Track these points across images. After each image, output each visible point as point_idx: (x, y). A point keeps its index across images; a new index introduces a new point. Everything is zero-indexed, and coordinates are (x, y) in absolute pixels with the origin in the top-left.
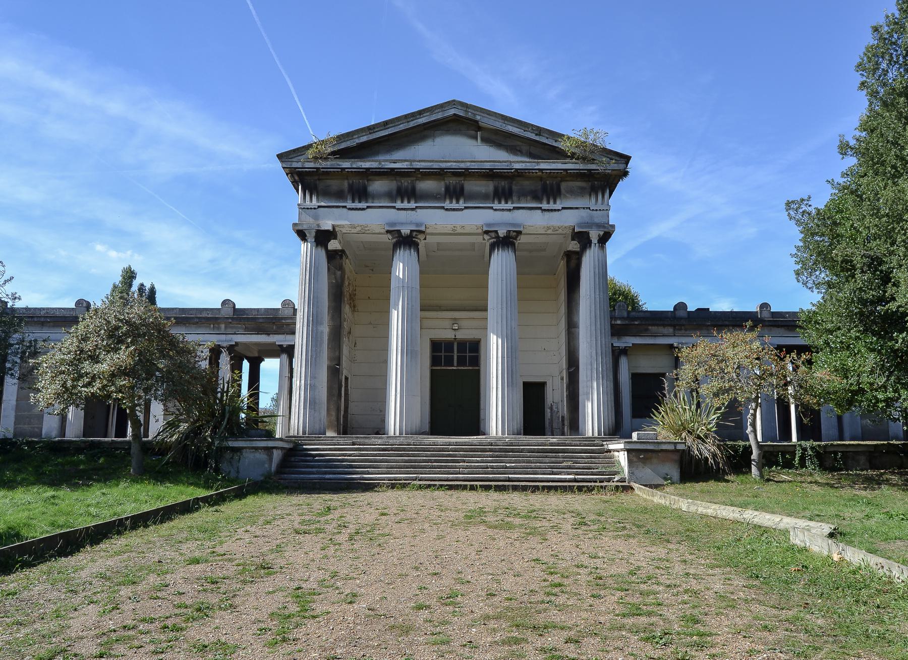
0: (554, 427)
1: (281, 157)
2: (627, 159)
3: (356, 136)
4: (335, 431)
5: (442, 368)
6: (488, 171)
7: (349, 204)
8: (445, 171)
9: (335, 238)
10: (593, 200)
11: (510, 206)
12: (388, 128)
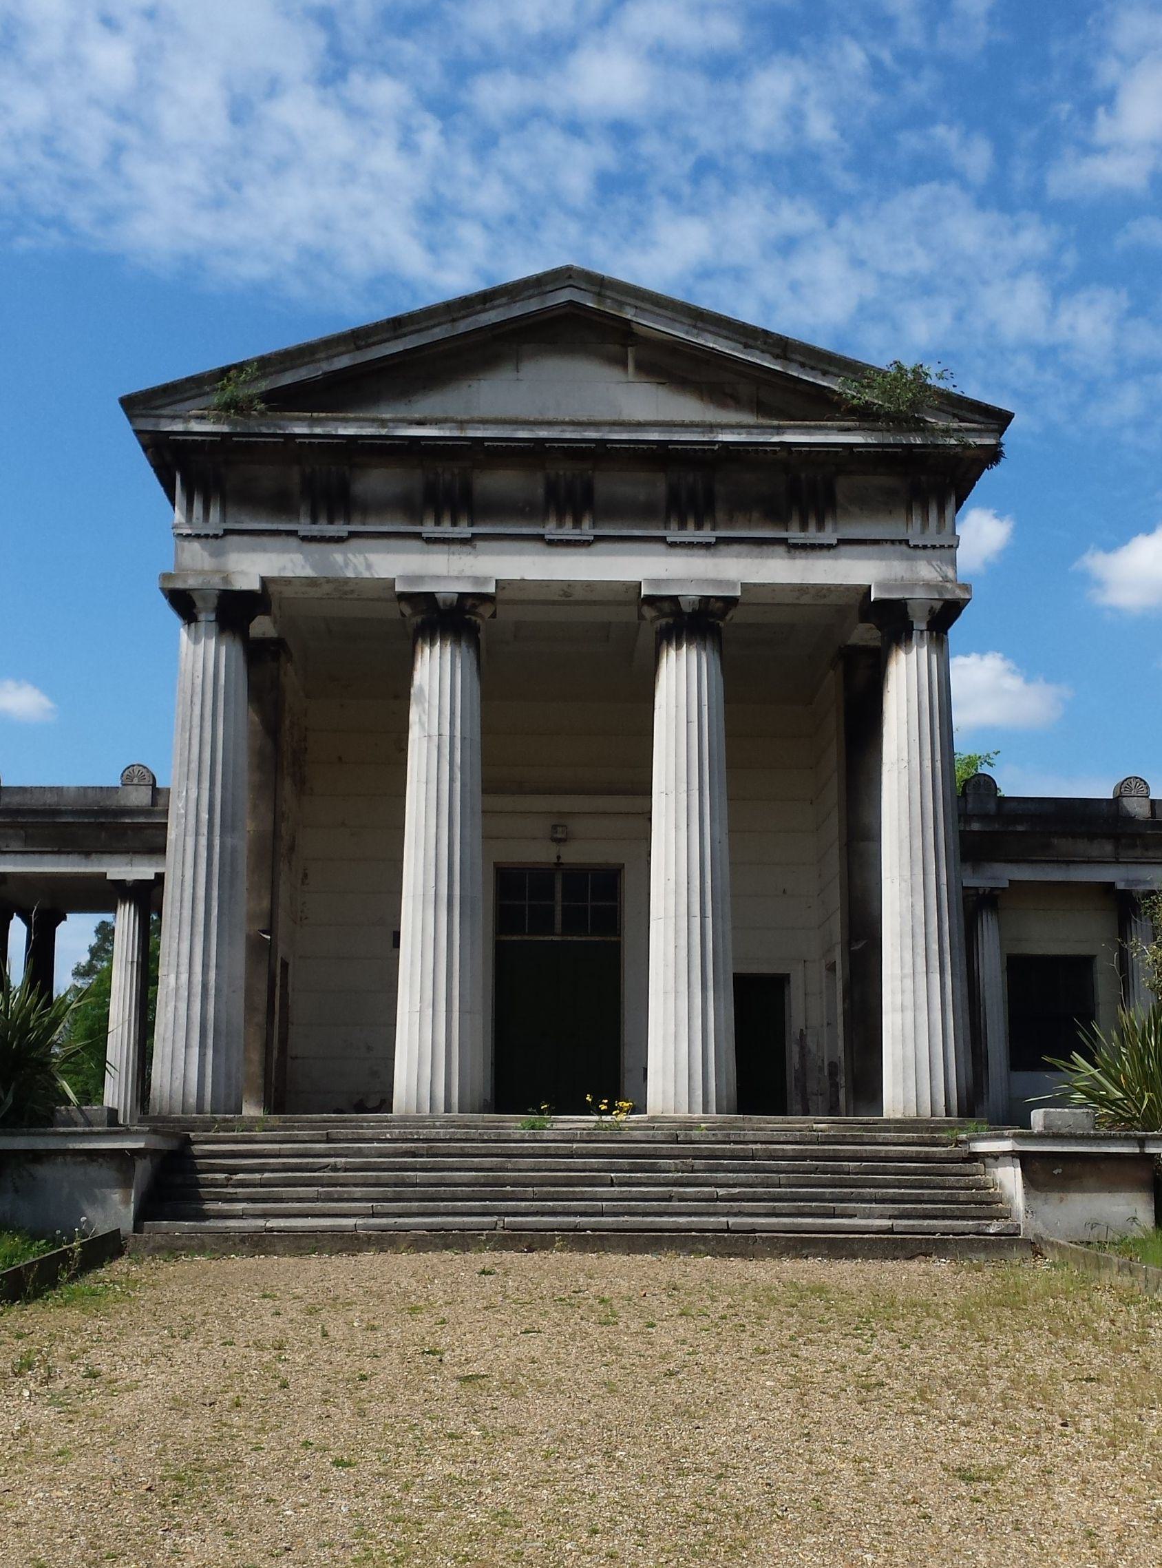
0: (809, 1090)
1: (133, 405)
2: (1001, 419)
3: (323, 355)
4: (257, 1104)
5: (526, 938)
6: (655, 447)
7: (305, 527)
8: (547, 445)
9: (266, 611)
10: (916, 522)
11: (707, 534)
12: (405, 335)
